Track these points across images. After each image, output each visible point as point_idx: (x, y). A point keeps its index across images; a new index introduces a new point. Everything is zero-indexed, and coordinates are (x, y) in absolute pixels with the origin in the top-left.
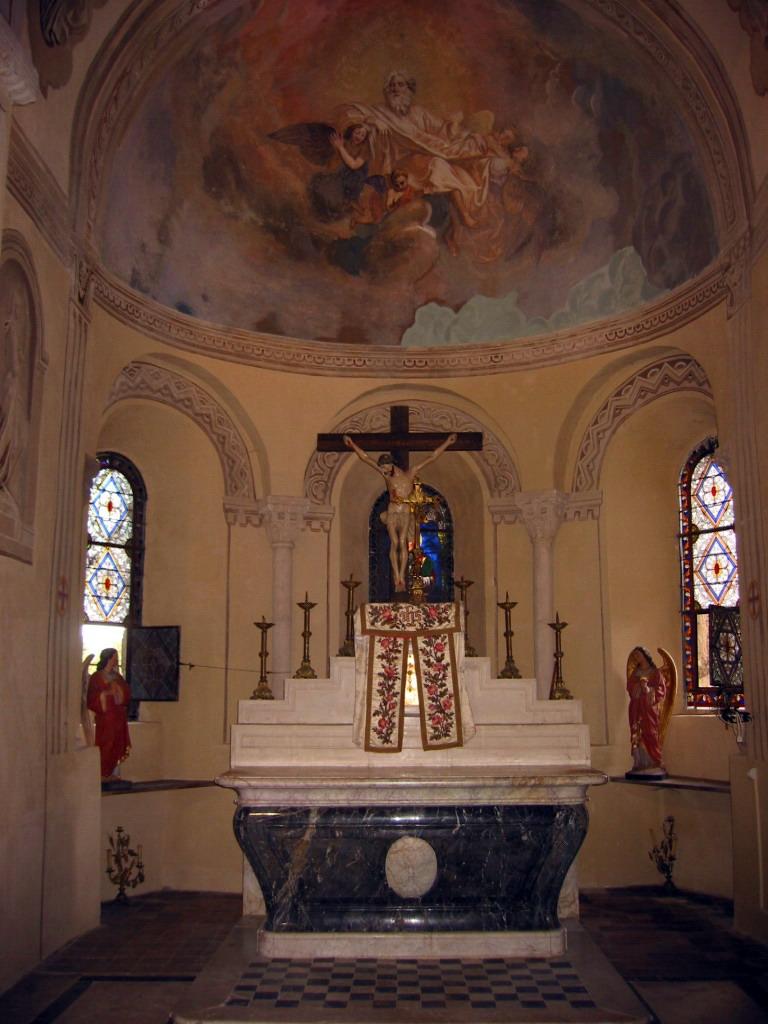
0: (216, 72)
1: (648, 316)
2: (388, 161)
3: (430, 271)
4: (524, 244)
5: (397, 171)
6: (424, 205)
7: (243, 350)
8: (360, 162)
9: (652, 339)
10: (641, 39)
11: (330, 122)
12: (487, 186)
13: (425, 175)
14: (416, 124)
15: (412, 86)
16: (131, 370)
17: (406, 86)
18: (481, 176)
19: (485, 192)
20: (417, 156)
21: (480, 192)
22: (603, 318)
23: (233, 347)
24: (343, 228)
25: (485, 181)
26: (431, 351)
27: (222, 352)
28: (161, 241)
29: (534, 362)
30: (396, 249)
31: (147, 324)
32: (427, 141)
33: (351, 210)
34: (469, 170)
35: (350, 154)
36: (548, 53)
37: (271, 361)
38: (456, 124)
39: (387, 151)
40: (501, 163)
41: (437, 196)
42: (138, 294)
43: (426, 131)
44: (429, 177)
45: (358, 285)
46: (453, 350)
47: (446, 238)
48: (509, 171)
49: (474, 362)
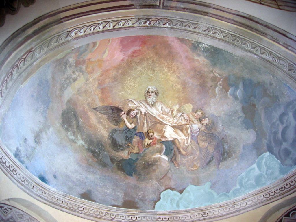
0: (73, 72)
1: (287, 182)
2: (145, 126)
3: (166, 175)
4: (210, 161)
5: (149, 131)
6: (162, 146)
7: (73, 207)
8: (133, 126)
9: (293, 192)
10: (264, 56)
11: (121, 107)
12: (190, 137)
13: (162, 133)
14: (158, 110)
15: (157, 93)
16: (6, 209)
17: (154, 93)
18: (187, 132)
19: (190, 139)
20: (158, 125)
21: (187, 140)
22: (259, 188)
23: (67, 205)
24: (124, 155)
25: (189, 135)
26: (170, 213)
27: (61, 206)
28: (35, 141)
29: (225, 215)
30: (149, 166)
31: (20, 181)
32: (163, 118)
33: (128, 147)
34: (182, 130)
35: (129, 122)
36: (217, 75)
37: (87, 215)
38: (175, 110)
39: (145, 122)
40: (196, 126)
41: (168, 142)
42: (16, 161)
43: (162, 114)
44: (164, 133)
45: (132, 180)
46: (181, 212)
47: (173, 160)
48: (200, 130)
49: (193, 218)
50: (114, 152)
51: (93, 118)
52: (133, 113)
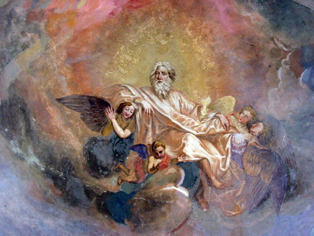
2: (150, 134)
8: (128, 133)
15: (172, 76)
19: (228, 160)
32: (181, 120)
50: (93, 179)
52: (129, 110)
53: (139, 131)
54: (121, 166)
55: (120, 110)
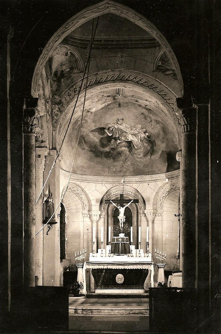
2: (117, 134)
8: (111, 134)
15: (123, 120)
19: (139, 141)
24: (107, 149)
30: (120, 154)
32: (126, 130)
47: (130, 150)
49: (136, 180)
50: (102, 148)
51: (91, 136)
52: (111, 129)
53: (92, 276)
54: (110, 144)
55: (109, 129)
